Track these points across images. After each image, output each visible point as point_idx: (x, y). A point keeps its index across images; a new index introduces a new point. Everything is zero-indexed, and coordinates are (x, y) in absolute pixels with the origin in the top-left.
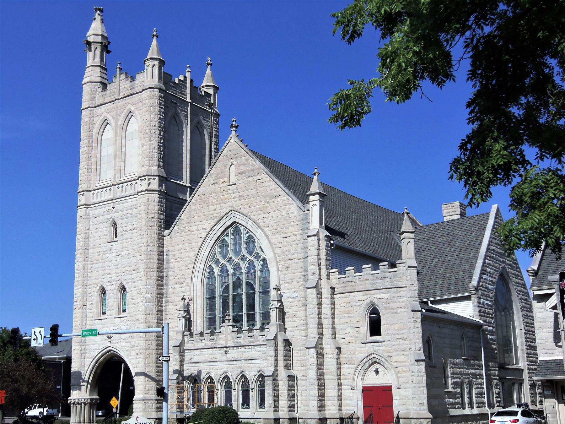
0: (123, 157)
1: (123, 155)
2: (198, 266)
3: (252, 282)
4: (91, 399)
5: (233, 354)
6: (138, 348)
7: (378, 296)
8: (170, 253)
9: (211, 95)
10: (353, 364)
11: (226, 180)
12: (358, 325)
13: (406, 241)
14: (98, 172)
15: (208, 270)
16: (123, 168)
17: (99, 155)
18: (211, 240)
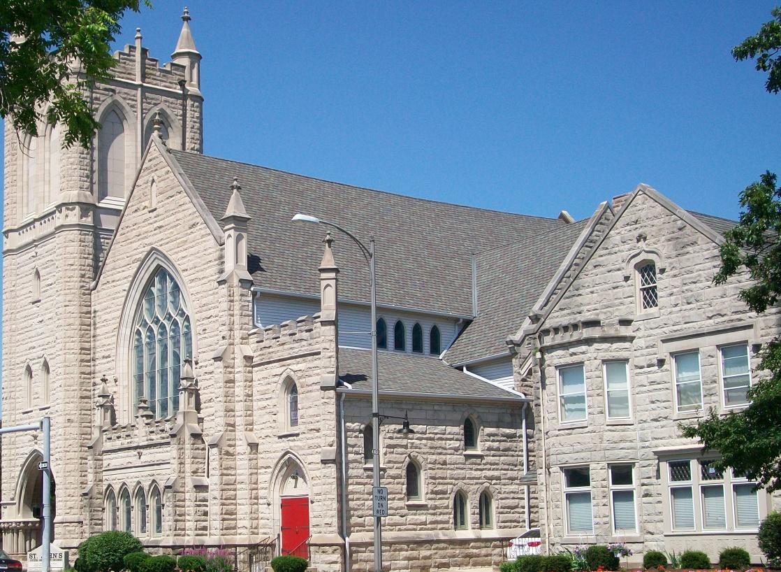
0: (47, 179)
1: (47, 175)
2: (124, 332)
3: (178, 352)
4: (24, 522)
5: (148, 455)
6: (59, 450)
7: (295, 367)
8: (97, 314)
9: (184, 67)
10: (269, 467)
11: (146, 203)
12: (274, 410)
13: (324, 283)
14: (25, 201)
15: (137, 337)
16: (47, 194)
17: (25, 177)
18: (136, 294)
